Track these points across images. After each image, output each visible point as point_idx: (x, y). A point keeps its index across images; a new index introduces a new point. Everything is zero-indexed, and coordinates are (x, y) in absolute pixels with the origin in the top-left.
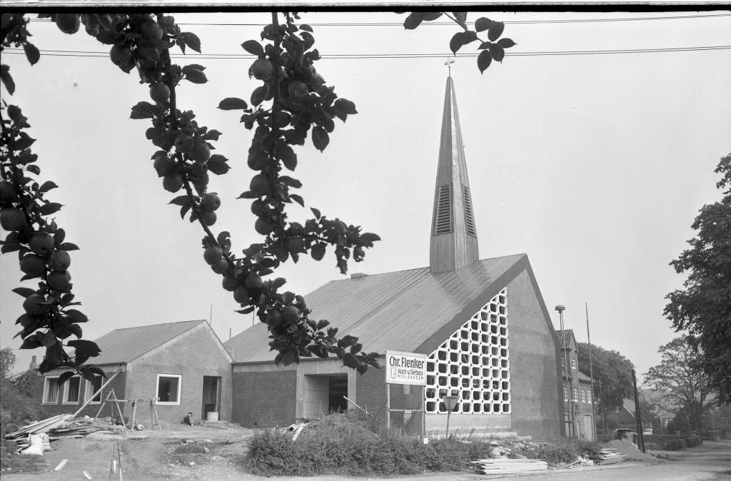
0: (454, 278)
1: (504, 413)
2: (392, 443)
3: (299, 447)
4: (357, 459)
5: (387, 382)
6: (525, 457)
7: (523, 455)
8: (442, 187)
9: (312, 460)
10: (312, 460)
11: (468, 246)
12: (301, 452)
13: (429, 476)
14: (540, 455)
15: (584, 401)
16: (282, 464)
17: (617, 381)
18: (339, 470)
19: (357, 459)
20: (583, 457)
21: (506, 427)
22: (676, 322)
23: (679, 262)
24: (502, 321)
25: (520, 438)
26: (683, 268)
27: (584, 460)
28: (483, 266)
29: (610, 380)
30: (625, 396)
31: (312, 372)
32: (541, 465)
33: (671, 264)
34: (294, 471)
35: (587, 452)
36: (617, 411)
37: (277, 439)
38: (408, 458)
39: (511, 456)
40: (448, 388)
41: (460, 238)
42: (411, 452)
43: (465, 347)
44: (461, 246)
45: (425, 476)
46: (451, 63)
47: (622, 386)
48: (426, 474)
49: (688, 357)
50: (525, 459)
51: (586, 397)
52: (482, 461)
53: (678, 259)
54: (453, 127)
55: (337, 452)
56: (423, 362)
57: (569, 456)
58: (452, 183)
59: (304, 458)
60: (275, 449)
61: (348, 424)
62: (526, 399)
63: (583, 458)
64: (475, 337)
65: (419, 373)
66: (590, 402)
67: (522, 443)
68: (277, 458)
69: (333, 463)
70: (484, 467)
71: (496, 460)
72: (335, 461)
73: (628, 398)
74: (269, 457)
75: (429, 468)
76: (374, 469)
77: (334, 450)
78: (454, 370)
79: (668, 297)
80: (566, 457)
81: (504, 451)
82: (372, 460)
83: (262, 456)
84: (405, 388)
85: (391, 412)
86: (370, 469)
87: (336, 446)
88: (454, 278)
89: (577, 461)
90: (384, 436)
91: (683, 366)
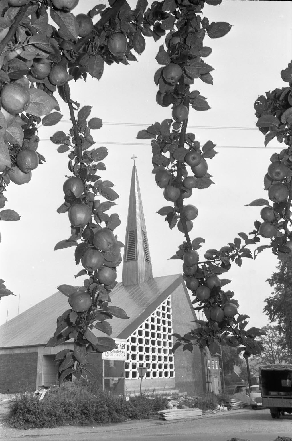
0: (137, 290)
1: (133, 378)
2: (107, 401)
3: (46, 407)
4: (84, 414)
5: (103, 359)
6: (188, 407)
7: (186, 405)
8: (130, 232)
9: (55, 416)
10: (55, 416)
11: (146, 269)
12: (47, 410)
13: (131, 423)
14: (195, 405)
15: (214, 368)
16: (35, 420)
17: (229, 354)
18: (72, 422)
19: (84, 414)
20: (220, 405)
21: (172, 387)
22: (270, 317)
23: (272, 280)
24: (169, 317)
25: (181, 394)
26: (274, 283)
27: (221, 408)
28: (155, 282)
29: (226, 354)
30: (235, 364)
31: (49, 353)
32: (198, 412)
33: (266, 281)
34: (43, 424)
35: (222, 402)
36: (230, 374)
37: (31, 401)
38: (117, 411)
39: (179, 407)
40: (144, 361)
41: (141, 264)
42: (119, 407)
43: (147, 334)
44: (142, 269)
45: (128, 424)
46: (135, 158)
47: (233, 357)
48: (128, 422)
49: (271, 338)
50: (188, 409)
51: (215, 365)
52: (164, 411)
53: (271, 278)
54: (137, 196)
55: (72, 409)
56: (125, 345)
57: (213, 405)
58: (136, 230)
59: (49, 414)
60: (30, 409)
61: (76, 388)
62: (183, 368)
63: (221, 406)
64: (153, 327)
65: (123, 352)
66: (217, 369)
67: (183, 398)
68: (31, 416)
69: (69, 417)
70: (165, 415)
71: (170, 410)
72: (70, 415)
73: (237, 365)
74: (26, 415)
75: (130, 417)
76: (95, 420)
77: (70, 408)
78: (141, 349)
79: (265, 301)
80: (210, 405)
81: (175, 404)
82: (96, 413)
83: (21, 415)
84: (110, 362)
85: (105, 380)
86: (93, 420)
87: (71, 405)
88: (137, 290)
89: (217, 408)
90: (101, 395)
91: (268, 344)
